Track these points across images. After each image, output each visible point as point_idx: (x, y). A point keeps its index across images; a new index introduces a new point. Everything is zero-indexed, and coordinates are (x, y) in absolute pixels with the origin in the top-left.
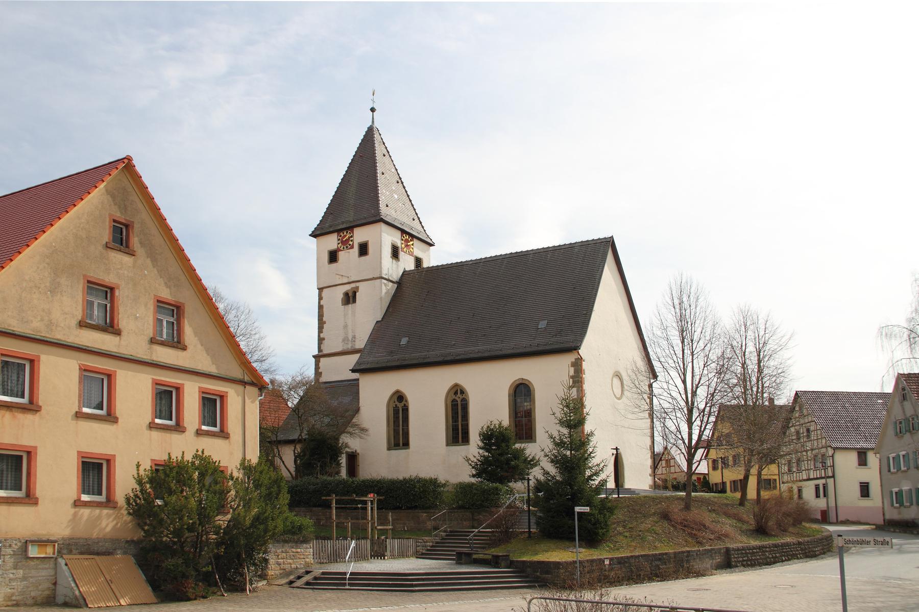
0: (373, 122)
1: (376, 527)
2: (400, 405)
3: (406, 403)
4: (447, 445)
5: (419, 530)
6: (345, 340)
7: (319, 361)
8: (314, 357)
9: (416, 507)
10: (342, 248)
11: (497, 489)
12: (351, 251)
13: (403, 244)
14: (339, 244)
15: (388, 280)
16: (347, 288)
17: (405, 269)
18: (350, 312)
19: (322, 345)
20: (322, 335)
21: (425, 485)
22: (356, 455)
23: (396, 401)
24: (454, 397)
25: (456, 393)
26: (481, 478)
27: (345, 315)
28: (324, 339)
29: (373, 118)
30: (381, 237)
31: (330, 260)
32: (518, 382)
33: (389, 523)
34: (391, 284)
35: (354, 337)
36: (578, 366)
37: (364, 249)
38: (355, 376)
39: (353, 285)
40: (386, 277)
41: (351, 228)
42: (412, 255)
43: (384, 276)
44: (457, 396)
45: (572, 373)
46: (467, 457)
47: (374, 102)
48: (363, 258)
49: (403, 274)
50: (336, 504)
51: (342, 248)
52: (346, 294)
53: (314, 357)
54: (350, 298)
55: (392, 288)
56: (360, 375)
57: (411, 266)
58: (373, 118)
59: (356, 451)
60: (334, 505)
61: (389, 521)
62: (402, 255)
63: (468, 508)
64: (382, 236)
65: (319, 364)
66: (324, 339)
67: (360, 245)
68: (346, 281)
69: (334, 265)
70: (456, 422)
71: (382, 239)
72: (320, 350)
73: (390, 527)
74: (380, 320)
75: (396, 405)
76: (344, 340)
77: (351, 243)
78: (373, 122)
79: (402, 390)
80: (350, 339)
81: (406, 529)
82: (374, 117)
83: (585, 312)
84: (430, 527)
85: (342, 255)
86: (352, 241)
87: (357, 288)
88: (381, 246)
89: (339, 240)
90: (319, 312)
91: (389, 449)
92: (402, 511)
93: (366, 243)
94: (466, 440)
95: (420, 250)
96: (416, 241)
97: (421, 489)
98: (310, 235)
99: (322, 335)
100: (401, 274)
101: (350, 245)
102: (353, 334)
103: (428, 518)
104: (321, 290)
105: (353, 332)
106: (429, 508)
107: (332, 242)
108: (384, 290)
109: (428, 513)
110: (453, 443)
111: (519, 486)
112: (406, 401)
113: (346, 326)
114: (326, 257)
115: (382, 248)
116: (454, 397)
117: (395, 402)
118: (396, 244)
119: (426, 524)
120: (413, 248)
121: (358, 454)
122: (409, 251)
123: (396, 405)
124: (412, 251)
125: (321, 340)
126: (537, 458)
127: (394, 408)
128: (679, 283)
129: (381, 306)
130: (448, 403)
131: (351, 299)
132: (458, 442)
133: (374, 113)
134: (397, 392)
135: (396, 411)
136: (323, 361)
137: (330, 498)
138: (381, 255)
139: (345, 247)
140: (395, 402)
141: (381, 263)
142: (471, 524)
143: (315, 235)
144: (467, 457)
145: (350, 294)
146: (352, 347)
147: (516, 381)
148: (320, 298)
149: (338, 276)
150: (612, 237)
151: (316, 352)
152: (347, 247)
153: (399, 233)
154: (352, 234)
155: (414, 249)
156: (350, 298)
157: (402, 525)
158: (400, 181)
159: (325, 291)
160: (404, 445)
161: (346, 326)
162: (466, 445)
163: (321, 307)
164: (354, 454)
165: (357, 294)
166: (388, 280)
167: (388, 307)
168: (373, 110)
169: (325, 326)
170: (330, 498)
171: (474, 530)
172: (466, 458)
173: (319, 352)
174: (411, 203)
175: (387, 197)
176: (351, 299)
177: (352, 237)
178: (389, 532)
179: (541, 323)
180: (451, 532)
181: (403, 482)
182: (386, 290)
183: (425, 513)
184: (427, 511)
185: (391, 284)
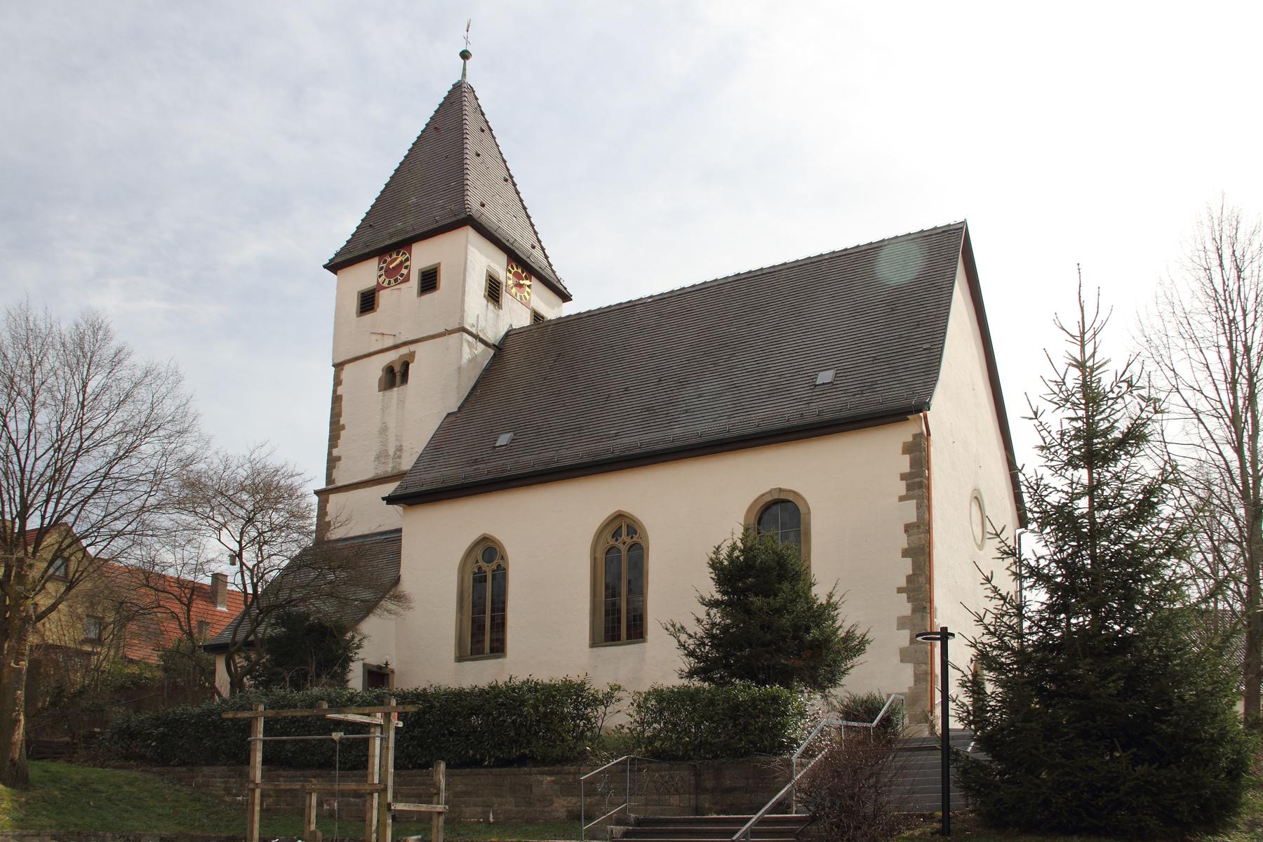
0: (464, 75)
1: (389, 805)
2: (488, 569)
3: (501, 562)
4: (594, 644)
5: (531, 821)
6: (381, 456)
7: (327, 501)
9: (522, 761)
10: (385, 284)
11: (775, 699)
12: (403, 286)
13: (510, 279)
14: (380, 276)
15: (476, 337)
17: (511, 325)
18: (394, 401)
20: (335, 452)
21: (554, 697)
22: (388, 674)
23: (480, 557)
24: (612, 542)
25: (616, 534)
26: (711, 680)
27: (384, 410)
28: (339, 459)
29: (464, 69)
30: (466, 254)
31: (361, 308)
32: (769, 498)
33: (438, 794)
34: (483, 346)
35: (400, 449)
36: (921, 452)
37: (429, 281)
38: (393, 517)
39: (404, 350)
40: (473, 330)
41: (405, 244)
42: (526, 305)
43: (468, 327)
46: (673, 626)
47: (468, 42)
48: (428, 297)
49: (507, 335)
50: (265, 734)
51: (385, 284)
52: (390, 370)
54: (395, 376)
55: (483, 355)
56: (404, 508)
57: (524, 320)
58: (464, 69)
59: (387, 664)
60: (261, 736)
61: (439, 789)
62: (506, 298)
63: (682, 758)
64: (469, 252)
65: (326, 507)
66: (339, 459)
67: (423, 273)
68: (389, 342)
69: (368, 317)
70: (614, 596)
71: (469, 257)
73: (440, 808)
74: (456, 410)
75: (480, 568)
76: (378, 458)
77: (404, 271)
78: (464, 75)
80: (391, 452)
81: (491, 820)
82: (467, 68)
83: (928, 346)
84: (562, 814)
85: (384, 297)
86: (406, 267)
88: (465, 269)
89: (381, 269)
90: (332, 409)
91: (460, 658)
92: (482, 770)
93: (436, 268)
94: (637, 632)
95: (543, 301)
96: (534, 282)
97: (541, 709)
98: (325, 267)
99: (335, 452)
100: (503, 333)
101: (402, 275)
102: (398, 444)
103: (556, 787)
104: (339, 366)
105: (397, 440)
106: (562, 760)
107: (367, 274)
108: (467, 354)
109: (559, 773)
110: (605, 641)
111: (813, 703)
112: (502, 558)
113: (384, 430)
114: (353, 303)
115: (467, 275)
116: (612, 542)
117: (477, 562)
118: (497, 275)
119: (552, 802)
120: (529, 294)
121: (393, 672)
122: (521, 297)
123: (480, 568)
124: (528, 297)
125: (332, 461)
126: (858, 633)
127: (475, 574)
128: (1216, 214)
129: (459, 384)
130: (598, 555)
131: (398, 378)
132: (620, 640)
133: (467, 61)
134: (485, 539)
135: (479, 579)
136: (334, 499)
137: (246, 714)
138: (464, 286)
139: (392, 280)
140: (477, 562)
141: (463, 301)
142: (693, 803)
143: (335, 266)
144: (673, 626)
145: (397, 369)
146: (394, 468)
147: (763, 495)
148: (337, 382)
150: (964, 222)
152: (396, 280)
153: (502, 258)
154: (408, 255)
155: (532, 295)
156: (395, 376)
157: (479, 809)
158: (509, 179)
159: (347, 371)
160: (492, 650)
161: (384, 430)
162: (641, 642)
163: (337, 400)
164: (383, 671)
165: (411, 365)
166: (476, 337)
167: (474, 388)
168: (465, 55)
169: (343, 433)
170: (246, 714)
171: (751, 816)
172: (672, 629)
173: (327, 485)
174: (526, 213)
176: (398, 378)
177: (407, 260)
178: (434, 822)
179: (821, 375)
180: (639, 822)
181: (488, 693)
182: (472, 355)
183: (550, 774)
184: (558, 768)
185: (481, 347)
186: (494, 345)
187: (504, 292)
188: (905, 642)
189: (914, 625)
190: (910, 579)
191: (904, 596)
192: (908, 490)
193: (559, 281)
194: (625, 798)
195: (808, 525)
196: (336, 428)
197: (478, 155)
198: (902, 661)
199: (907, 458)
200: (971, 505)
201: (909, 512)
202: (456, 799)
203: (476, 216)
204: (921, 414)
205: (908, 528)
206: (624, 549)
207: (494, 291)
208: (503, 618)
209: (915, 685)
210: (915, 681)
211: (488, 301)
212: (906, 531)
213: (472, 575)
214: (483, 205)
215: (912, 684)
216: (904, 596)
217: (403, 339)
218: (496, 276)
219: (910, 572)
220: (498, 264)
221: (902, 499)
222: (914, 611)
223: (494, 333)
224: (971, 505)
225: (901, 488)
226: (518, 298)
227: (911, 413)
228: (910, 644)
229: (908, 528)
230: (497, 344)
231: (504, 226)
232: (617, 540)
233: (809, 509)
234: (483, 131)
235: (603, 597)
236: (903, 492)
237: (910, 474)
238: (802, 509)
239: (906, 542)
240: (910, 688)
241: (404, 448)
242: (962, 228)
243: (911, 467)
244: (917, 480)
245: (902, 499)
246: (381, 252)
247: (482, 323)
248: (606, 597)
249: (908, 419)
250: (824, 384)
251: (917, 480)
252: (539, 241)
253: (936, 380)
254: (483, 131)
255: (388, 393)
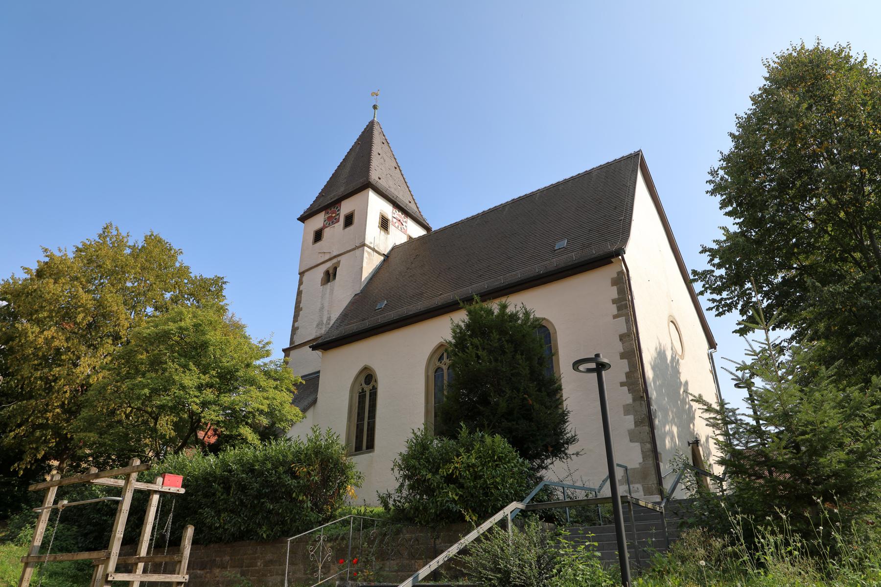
2: (367, 388)
8: (284, 350)
12: (336, 225)
15: (374, 250)
16: (328, 265)
18: (328, 291)
19: (295, 336)
20: (296, 325)
24: (438, 364)
37: (349, 220)
44: (443, 362)
45: (615, 295)
49: (393, 249)
52: (327, 273)
53: (284, 350)
54: (330, 276)
62: (391, 228)
68: (327, 257)
69: (318, 244)
72: (292, 341)
76: (318, 325)
79: (372, 366)
85: (327, 233)
87: (339, 262)
98: (298, 219)
99: (296, 325)
104: (302, 274)
113: (322, 308)
114: (311, 237)
116: (438, 364)
117: (361, 385)
122: (401, 228)
124: (405, 228)
125: (294, 330)
127: (360, 393)
134: (366, 368)
135: (362, 396)
143: (303, 219)
145: (331, 272)
148: (301, 283)
149: (320, 255)
150: (640, 151)
151: (287, 346)
160: (367, 448)
163: (299, 293)
166: (374, 250)
168: (375, 107)
175: (378, 171)
186: (384, 254)
187: (391, 225)
188: (632, 426)
189: (636, 411)
190: (628, 375)
191: (626, 388)
192: (618, 310)
193: (424, 220)
194: (279, 578)
195: (556, 341)
196: (298, 309)
197: (379, 154)
198: (631, 441)
199: (615, 288)
200: (669, 326)
201: (621, 326)
202: (265, 568)
203: (374, 183)
204: (620, 257)
205: (622, 338)
206: (445, 368)
207: (384, 224)
208: (374, 422)
209: (644, 461)
210: (643, 458)
211: (381, 230)
212: (621, 340)
213: (358, 395)
214: (380, 179)
215: (641, 460)
216: (626, 388)
217: (335, 254)
218: (386, 216)
219: (628, 370)
220: (388, 210)
221: (615, 317)
222: (634, 400)
223: (386, 249)
224: (669, 326)
225: (614, 309)
226: (400, 228)
227: (613, 257)
228: (635, 427)
229: (622, 338)
230: (386, 254)
231: (392, 190)
232: (441, 363)
233: (555, 329)
234: (383, 143)
235: (433, 403)
236: (615, 312)
237: (619, 299)
238: (550, 328)
239: (622, 348)
240: (640, 463)
241: (332, 318)
242: (639, 154)
243: (618, 293)
244: (623, 303)
245: (615, 317)
246: (325, 208)
247: (377, 242)
248: (435, 404)
249: (612, 262)
250: (560, 249)
251: (623, 303)
252: (414, 200)
253: (629, 236)
254: (383, 143)
255: (325, 286)
